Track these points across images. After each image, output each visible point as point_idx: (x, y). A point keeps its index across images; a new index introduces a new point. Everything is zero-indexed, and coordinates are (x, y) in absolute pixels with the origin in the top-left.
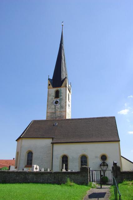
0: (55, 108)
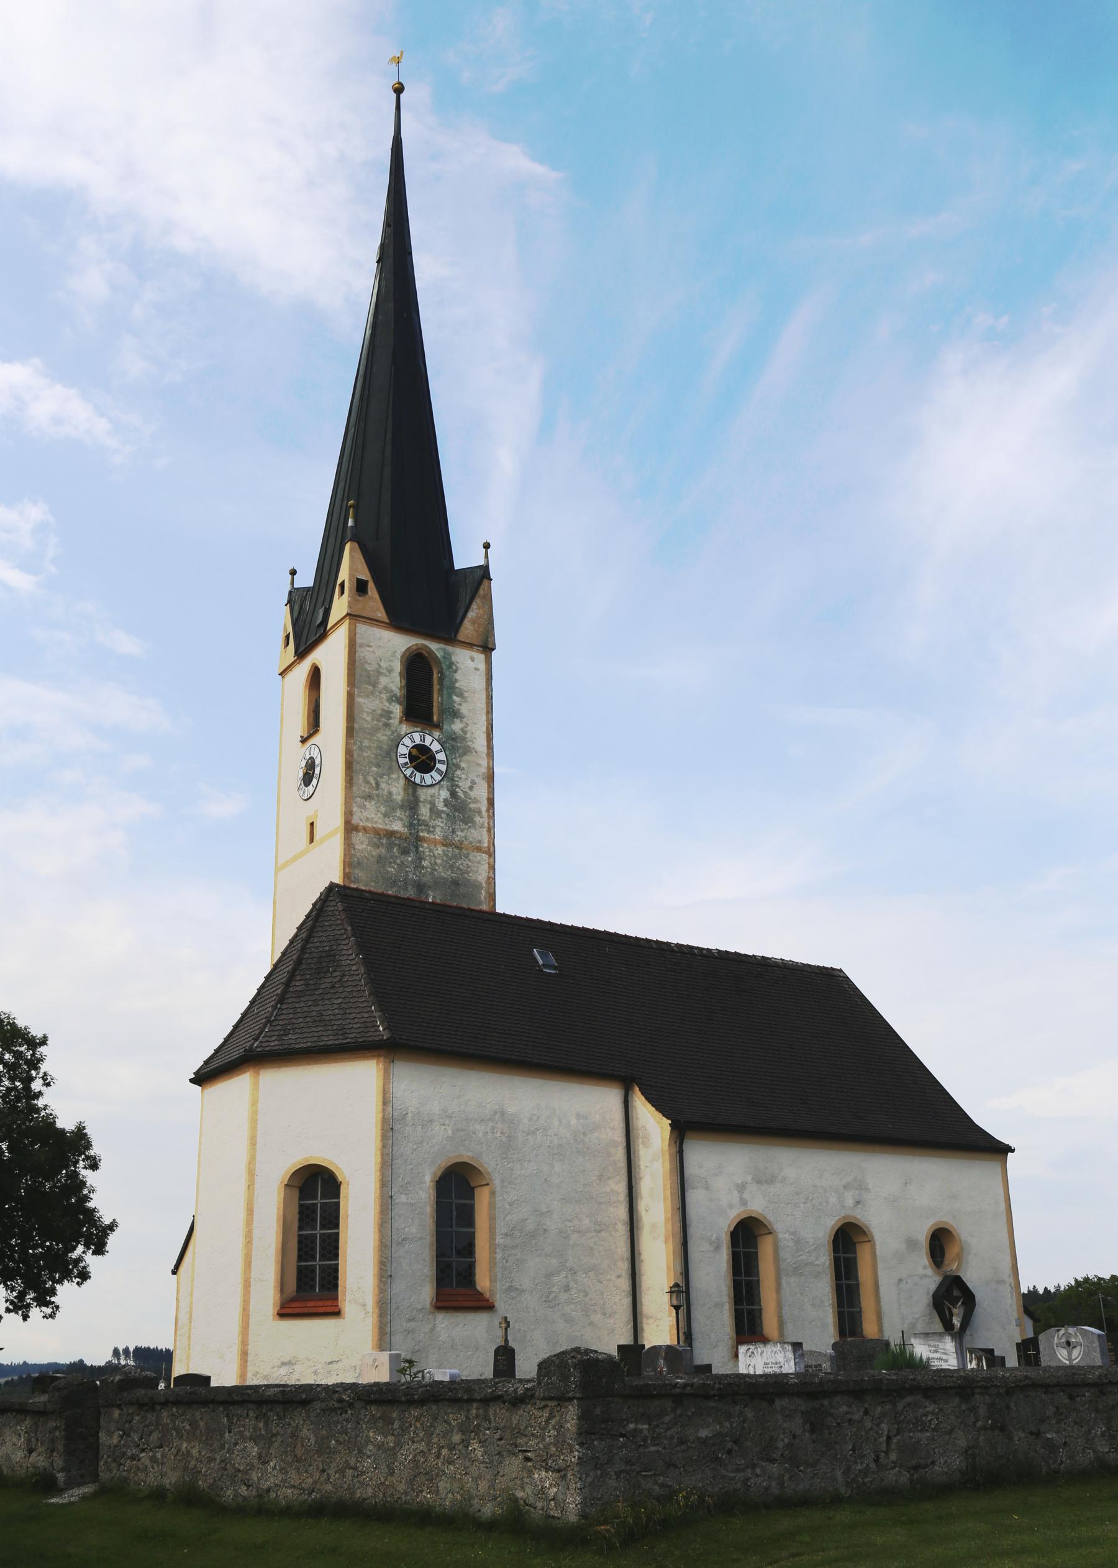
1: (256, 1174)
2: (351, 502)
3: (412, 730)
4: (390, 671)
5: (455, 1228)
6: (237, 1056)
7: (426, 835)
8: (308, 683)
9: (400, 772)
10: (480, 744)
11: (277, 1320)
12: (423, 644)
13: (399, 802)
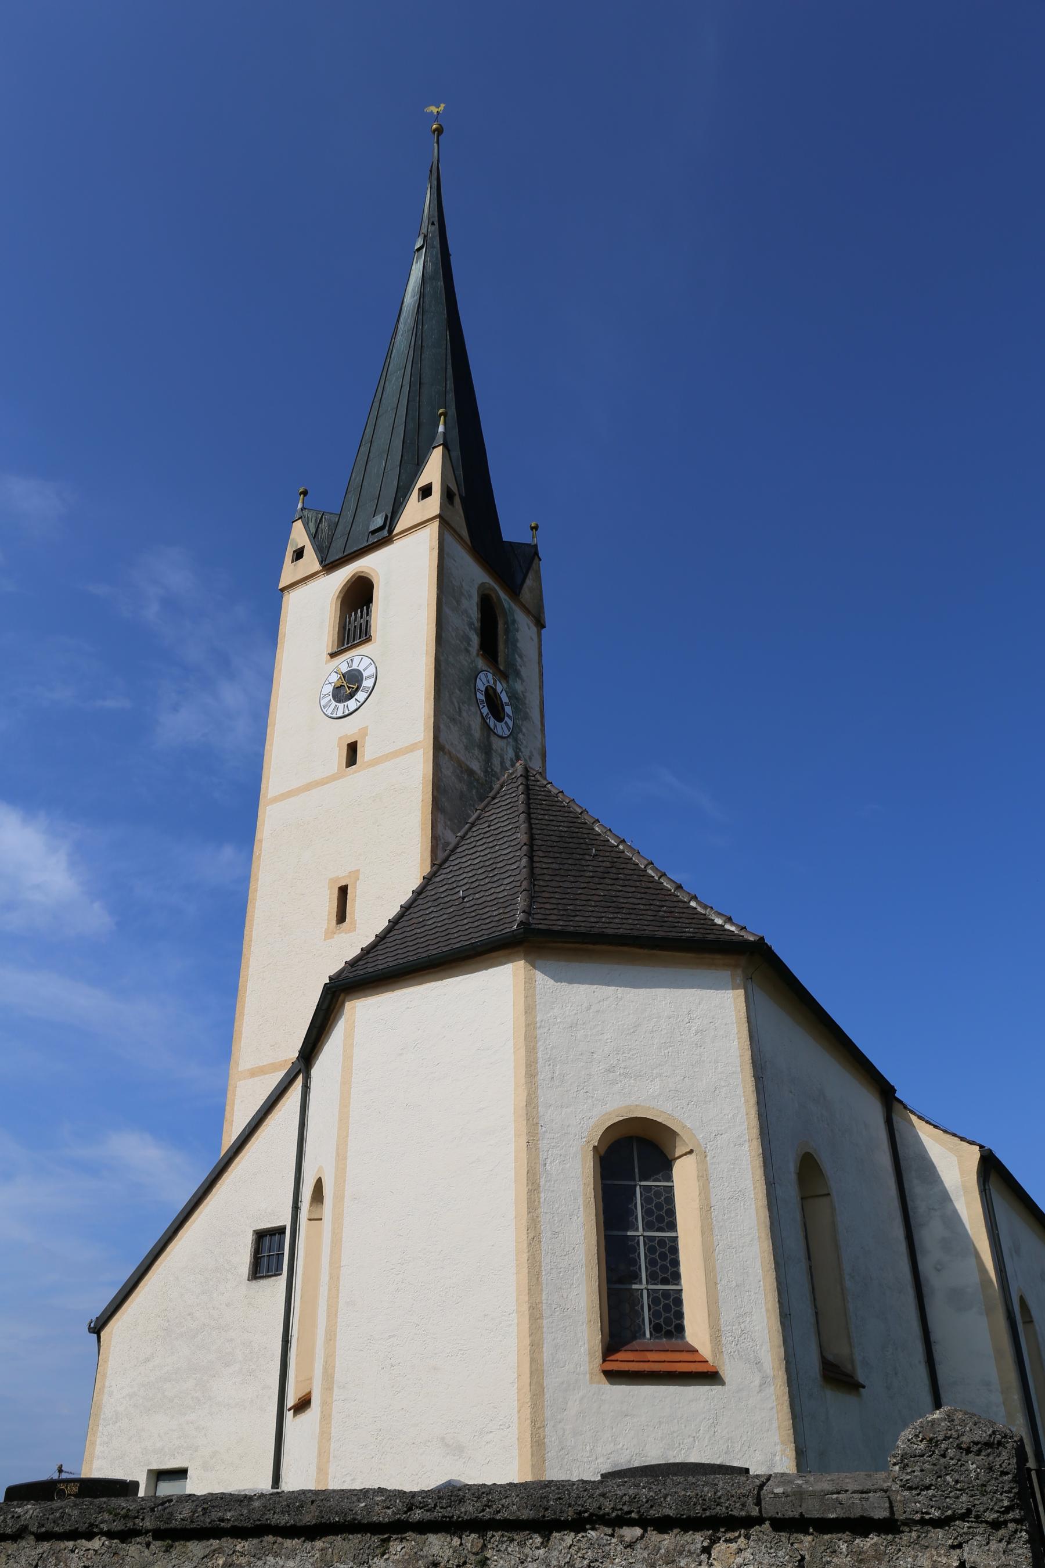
0: (487, 750)
1: (541, 1123)
2: (441, 411)
3: (486, 669)
4: (470, 596)
5: (643, 1286)
6: (485, 937)
7: (475, 797)
8: (342, 595)
9: (478, 708)
10: (535, 714)
11: (599, 1383)
12: (494, 587)
13: (477, 740)
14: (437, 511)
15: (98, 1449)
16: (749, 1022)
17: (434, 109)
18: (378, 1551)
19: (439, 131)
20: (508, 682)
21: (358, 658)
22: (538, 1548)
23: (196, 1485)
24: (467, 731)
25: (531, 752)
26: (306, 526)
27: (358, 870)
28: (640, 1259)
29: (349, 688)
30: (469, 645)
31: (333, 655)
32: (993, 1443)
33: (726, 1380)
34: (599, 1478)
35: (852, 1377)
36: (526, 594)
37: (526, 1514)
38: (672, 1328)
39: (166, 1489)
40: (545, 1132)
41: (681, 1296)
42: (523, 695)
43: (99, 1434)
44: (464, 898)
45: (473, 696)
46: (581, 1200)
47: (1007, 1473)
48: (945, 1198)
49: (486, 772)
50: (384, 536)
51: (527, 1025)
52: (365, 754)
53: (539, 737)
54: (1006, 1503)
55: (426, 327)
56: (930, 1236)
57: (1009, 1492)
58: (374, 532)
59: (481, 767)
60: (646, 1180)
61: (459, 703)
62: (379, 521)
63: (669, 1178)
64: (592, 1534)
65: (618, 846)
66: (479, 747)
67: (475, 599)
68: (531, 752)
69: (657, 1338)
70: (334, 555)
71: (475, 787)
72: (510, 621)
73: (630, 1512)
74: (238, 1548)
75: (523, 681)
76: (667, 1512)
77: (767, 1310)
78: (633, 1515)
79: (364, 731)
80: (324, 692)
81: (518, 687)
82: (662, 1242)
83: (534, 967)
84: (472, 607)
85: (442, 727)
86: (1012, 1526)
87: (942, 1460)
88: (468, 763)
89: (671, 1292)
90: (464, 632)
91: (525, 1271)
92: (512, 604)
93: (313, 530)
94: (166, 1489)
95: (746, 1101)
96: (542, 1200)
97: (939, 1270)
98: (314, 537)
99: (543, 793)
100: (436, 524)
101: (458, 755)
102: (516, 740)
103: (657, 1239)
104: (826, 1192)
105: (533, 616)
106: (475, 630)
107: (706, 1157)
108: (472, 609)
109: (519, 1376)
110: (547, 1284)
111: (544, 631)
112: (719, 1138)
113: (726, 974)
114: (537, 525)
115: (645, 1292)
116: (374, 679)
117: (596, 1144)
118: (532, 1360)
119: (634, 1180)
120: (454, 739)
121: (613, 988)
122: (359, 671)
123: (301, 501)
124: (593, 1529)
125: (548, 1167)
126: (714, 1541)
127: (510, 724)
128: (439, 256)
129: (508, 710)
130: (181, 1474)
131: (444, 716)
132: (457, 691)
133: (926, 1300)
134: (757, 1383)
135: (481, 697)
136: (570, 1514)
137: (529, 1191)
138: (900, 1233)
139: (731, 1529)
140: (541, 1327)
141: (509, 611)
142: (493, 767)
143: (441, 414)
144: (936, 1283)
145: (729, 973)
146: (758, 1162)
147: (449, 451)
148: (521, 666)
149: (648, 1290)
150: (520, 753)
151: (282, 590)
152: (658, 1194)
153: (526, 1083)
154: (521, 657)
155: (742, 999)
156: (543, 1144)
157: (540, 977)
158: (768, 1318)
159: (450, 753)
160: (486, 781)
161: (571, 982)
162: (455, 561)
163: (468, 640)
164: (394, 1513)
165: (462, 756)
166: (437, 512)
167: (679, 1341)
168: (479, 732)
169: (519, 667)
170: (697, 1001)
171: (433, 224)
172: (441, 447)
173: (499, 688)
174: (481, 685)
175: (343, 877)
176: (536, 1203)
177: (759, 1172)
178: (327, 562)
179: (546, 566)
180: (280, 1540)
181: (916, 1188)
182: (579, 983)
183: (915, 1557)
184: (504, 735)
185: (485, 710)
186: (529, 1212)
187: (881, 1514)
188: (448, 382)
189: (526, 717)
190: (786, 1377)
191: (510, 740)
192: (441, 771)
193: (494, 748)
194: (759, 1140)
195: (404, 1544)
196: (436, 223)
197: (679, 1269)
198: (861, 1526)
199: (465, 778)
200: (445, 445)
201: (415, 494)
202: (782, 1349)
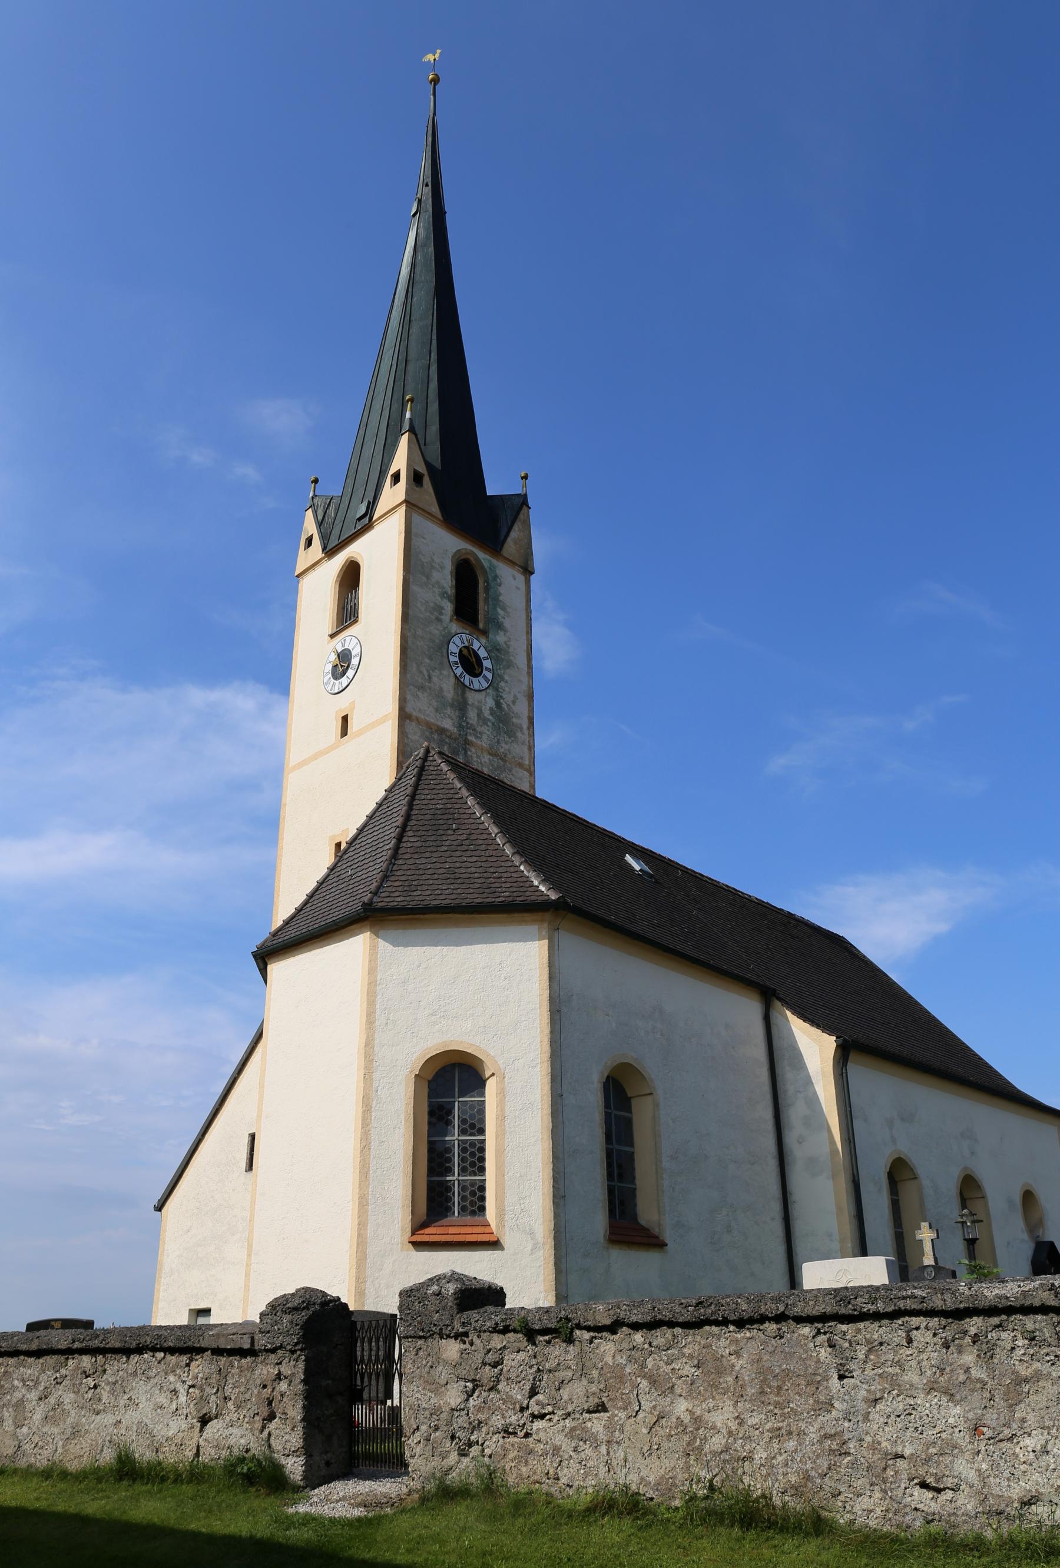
0: (461, 706)
1: (376, 1059)
3: (461, 631)
4: (442, 568)
8: (339, 579)
9: (451, 670)
10: (521, 660)
11: (407, 1250)
13: (450, 700)
14: (402, 497)
15: (161, 1294)
16: (550, 967)
17: (430, 57)
18: (63, 1365)
19: (436, 81)
20: (487, 637)
21: (349, 639)
22: (124, 1363)
23: (214, 1319)
24: (439, 695)
25: (515, 696)
26: (315, 513)
27: (348, 829)
28: (454, 1157)
29: (342, 666)
30: (441, 614)
31: (332, 636)
32: (300, 1308)
33: (505, 1247)
34: (23, 1329)
35: (658, 1237)
36: (510, 547)
37: (118, 1345)
38: (475, 1208)
39: (202, 1321)
40: (378, 1066)
41: (485, 1184)
42: (506, 644)
43: (162, 1284)
44: (351, 875)
45: (446, 660)
46: (402, 1117)
47: (298, 1325)
48: (808, 1082)
49: (460, 727)
50: (366, 523)
51: (369, 984)
52: (353, 726)
53: (525, 680)
54: (295, 1341)
55: (415, 300)
56: (794, 1115)
57: (297, 1335)
58: (360, 519)
59: (454, 723)
60: (463, 1097)
61: (428, 671)
62: (363, 509)
63: (483, 1095)
64: (146, 1355)
65: (480, 817)
66: (452, 706)
67: (449, 566)
68: (515, 696)
69: (463, 1216)
70: (333, 543)
71: (446, 743)
72: (490, 578)
73: (157, 1344)
74: (10, 1363)
75: (505, 631)
76: (171, 1344)
77: (543, 1194)
78: (158, 1346)
79: (353, 705)
80: (326, 671)
81: (501, 638)
82: (472, 1144)
83: (378, 937)
84: (445, 579)
85: (409, 697)
86: (298, 1352)
87: (275, 1317)
88: (439, 723)
89: (477, 1182)
90: (435, 603)
91: (358, 1170)
92: (494, 561)
93: (320, 518)
94: (202, 1321)
95: (541, 1031)
96: (373, 1118)
97: (800, 1143)
98: (320, 525)
99: (435, 773)
100: (403, 508)
101: (427, 719)
102: (497, 690)
103: (469, 1142)
104: (649, 1092)
105: (519, 566)
106: (449, 598)
107: (504, 1078)
108: (444, 579)
109: (351, 1246)
110: (373, 1180)
111: (532, 577)
112: (516, 1062)
113: (533, 929)
114: (527, 474)
115: (456, 1182)
116: (359, 658)
117: (417, 1073)
118: (359, 1235)
119: (454, 1097)
120: (423, 706)
121: (440, 948)
122: (349, 650)
123: (312, 489)
124: (146, 1353)
125: (379, 1093)
126: (191, 1360)
127: (489, 676)
128: (431, 219)
129: (487, 664)
130: (206, 1312)
131: (412, 687)
132: (427, 661)
133: (787, 1168)
134: (529, 1248)
135: (454, 659)
136: (134, 1345)
137: (364, 1112)
138: (768, 1114)
139: (73, 1354)
140: (367, 1211)
141: (490, 569)
142: (468, 720)
143: (408, 400)
144: (797, 1152)
145: (537, 927)
146: (547, 1080)
147: (416, 435)
148: (504, 618)
149: (459, 1181)
150: (502, 701)
151: (298, 576)
152: (472, 1107)
153: (366, 1029)
154: (504, 609)
155: (546, 947)
156: (376, 1075)
157: (381, 943)
158: (543, 1200)
159: (417, 719)
160: (460, 734)
161: (406, 946)
162: (425, 538)
163: (440, 609)
164: (68, 1344)
165: (432, 718)
166: (403, 498)
167: (481, 1218)
168: (452, 692)
169: (501, 620)
170: (508, 952)
171: (427, 185)
172: (407, 433)
173: (476, 645)
174: (453, 648)
175: (338, 835)
176: (369, 1120)
177: (547, 1088)
178: (327, 550)
179: (535, 513)
180: (26, 1358)
181: (787, 1074)
182: (413, 946)
183: (262, 1369)
184: (482, 688)
185: (459, 670)
186: (362, 1128)
187: (247, 1346)
188: (432, 355)
189: (510, 665)
190: (553, 1243)
191: (489, 691)
192: (408, 738)
193: (470, 702)
194: (549, 1062)
195: (74, 1361)
196: (430, 184)
197: (485, 1164)
198: (241, 1353)
199: (436, 737)
200: (412, 430)
201: (388, 480)
202: (553, 1223)
